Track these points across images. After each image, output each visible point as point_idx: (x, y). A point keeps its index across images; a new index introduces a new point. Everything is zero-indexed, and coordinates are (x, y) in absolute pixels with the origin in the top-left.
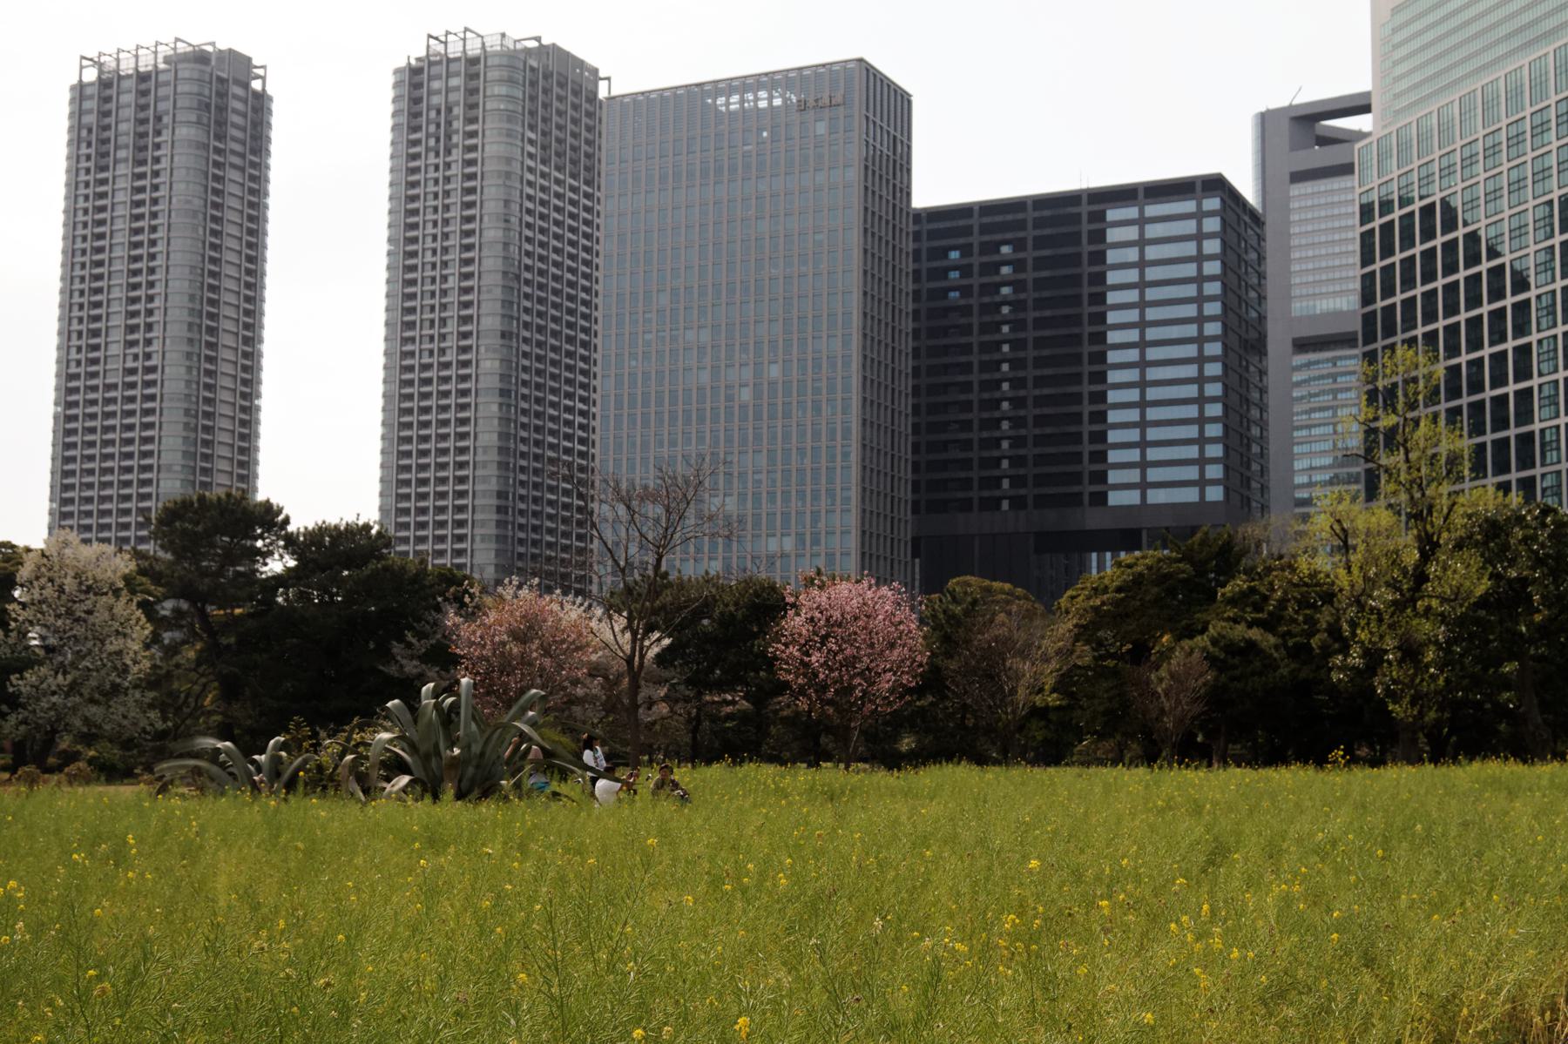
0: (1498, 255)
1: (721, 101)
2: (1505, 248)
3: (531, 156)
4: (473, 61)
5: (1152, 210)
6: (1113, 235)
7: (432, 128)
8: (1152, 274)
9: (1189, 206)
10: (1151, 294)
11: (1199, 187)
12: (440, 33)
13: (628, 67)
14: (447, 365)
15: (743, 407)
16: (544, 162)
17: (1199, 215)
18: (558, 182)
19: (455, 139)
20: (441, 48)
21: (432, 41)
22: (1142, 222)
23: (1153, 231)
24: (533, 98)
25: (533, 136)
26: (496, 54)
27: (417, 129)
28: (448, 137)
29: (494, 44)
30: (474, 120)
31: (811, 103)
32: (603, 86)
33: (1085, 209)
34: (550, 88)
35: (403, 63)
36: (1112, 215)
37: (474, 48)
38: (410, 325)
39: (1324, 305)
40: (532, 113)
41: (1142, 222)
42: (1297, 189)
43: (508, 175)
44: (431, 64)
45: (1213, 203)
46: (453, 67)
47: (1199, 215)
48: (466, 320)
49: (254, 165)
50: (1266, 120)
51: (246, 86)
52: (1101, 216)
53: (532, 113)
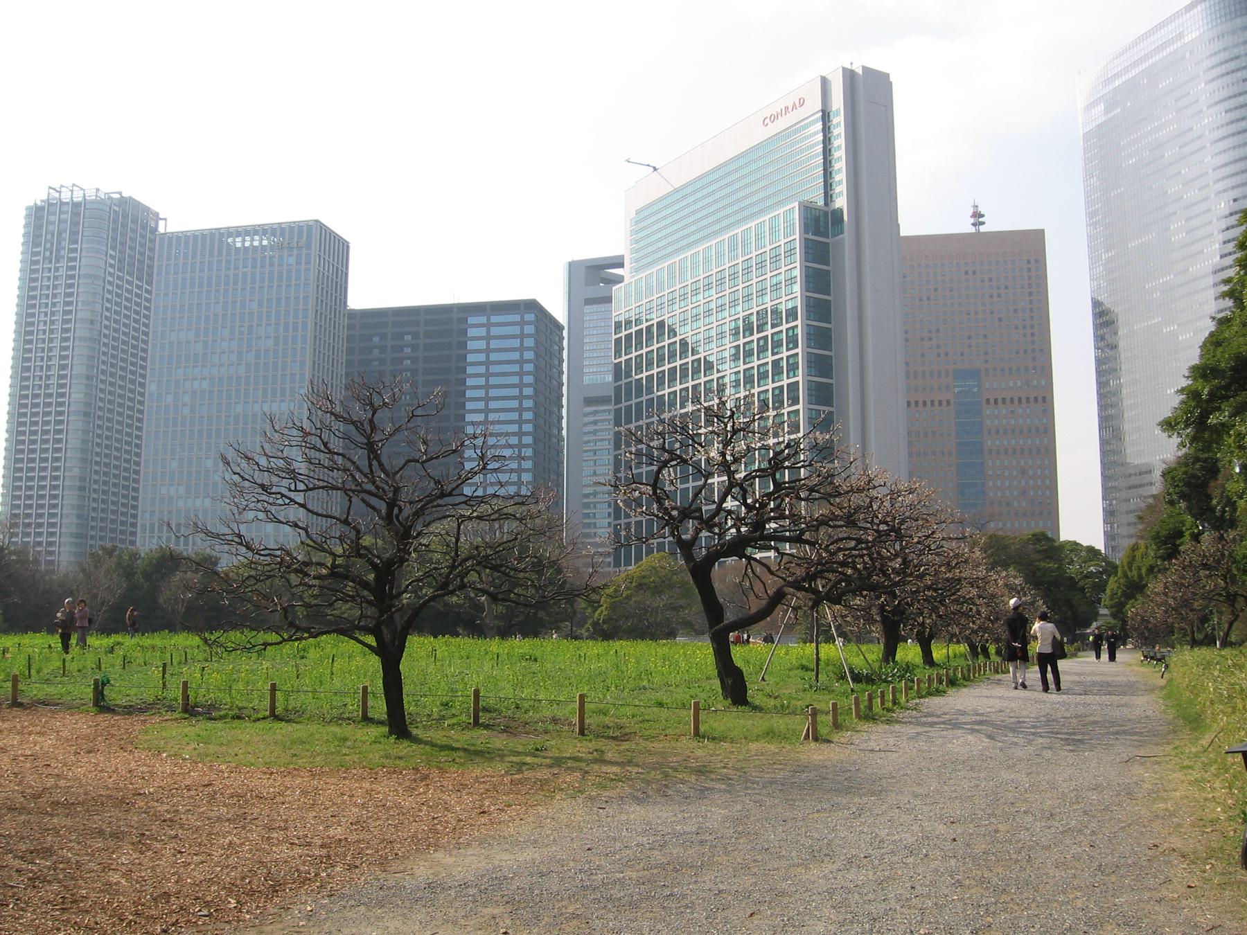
0: (698, 353)
1: (230, 240)
2: (701, 349)
3: (111, 266)
5: (494, 319)
6: (472, 332)
7: (48, 245)
8: (494, 357)
9: (517, 318)
10: (493, 369)
12: (57, 186)
13: (180, 215)
14: (50, 395)
15: (237, 417)
16: (119, 270)
17: (522, 323)
18: (128, 282)
19: (62, 253)
20: (57, 195)
22: (488, 325)
23: (495, 331)
26: (92, 202)
27: (39, 245)
29: (91, 195)
30: (76, 242)
31: (286, 244)
32: (161, 223)
35: (31, 204)
36: (471, 320)
37: (78, 198)
38: (28, 369)
39: (599, 379)
40: (114, 239)
42: (588, 309)
43: (92, 322)
44: (50, 205)
45: (530, 317)
46: (64, 208)
48: (63, 367)
50: (573, 267)
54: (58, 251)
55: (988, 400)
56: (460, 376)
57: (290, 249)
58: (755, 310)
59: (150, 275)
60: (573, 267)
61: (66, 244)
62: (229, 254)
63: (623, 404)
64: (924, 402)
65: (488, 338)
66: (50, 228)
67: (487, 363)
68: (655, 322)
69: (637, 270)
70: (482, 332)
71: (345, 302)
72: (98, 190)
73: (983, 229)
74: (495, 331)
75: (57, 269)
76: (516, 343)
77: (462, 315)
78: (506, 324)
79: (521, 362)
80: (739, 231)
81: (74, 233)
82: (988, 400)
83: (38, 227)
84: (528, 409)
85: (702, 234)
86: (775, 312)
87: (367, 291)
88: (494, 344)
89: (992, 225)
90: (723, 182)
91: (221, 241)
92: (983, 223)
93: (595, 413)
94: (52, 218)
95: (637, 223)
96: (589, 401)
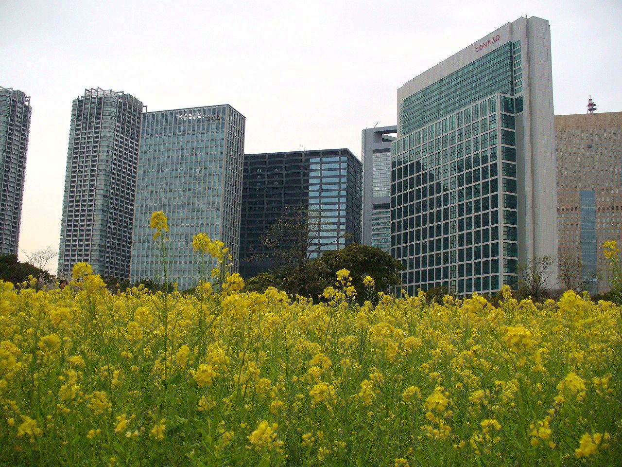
1: (181, 116)
3: (117, 131)
4: (100, 99)
5: (325, 159)
7: (85, 121)
8: (324, 181)
9: (337, 159)
10: (324, 187)
11: (340, 153)
18: (127, 140)
21: (87, 92)
23: (325, 166)
24: (119, 112)
25: (119, 125)
27: (79, 120)
28: (90, 123)
29: (107, 93)
30: (99, 119)
31: (211, 118)
33: (303, 158)
34: (128, 107)
36: (312, 160)
38: (73, 187)
41: (321, 163)
45: (344, 158)
47: (340, 162)
49: (24, 130)
50: (366, 132)
51: (22, 103)
52: (308, 160)
53: (119, 117)
54: (90, 123)
55: (599, 208)
56: (305, 191)
57: (214, 120)
58: (456, 160)
59: (138, 136)
60: (366, 132)
61: (94, 120)
62: (180, 123)
63: (396, 208)
64: (572, 208)
65: (321, 170)
66: (86, 111)
67: (321, 184)
68: (415, 161)
69: (404, 133)
70: (318, 167)
71: (243, 150)
72: (111, 90)
73: (595, 112)
74: (325, 166)
75: (89, 133)
76: (336, 173)
77: (307, 157)
78: (332, 197)
79: (340, 183)
80: (463, 109)
81: (99, 114)
82: (599, 208)
83: (80, 111)
84: (343, 210)
85: (483, 93)
86: (100, 251)
87: (255, 144)
88: (324, 173)
89: (599, 110)
90: (496, 61)
91: (176, 117)
92: (595, 109)
93: (379, 213)
94: (87, 106)
95: (404, 107)
96: (376, 207)
